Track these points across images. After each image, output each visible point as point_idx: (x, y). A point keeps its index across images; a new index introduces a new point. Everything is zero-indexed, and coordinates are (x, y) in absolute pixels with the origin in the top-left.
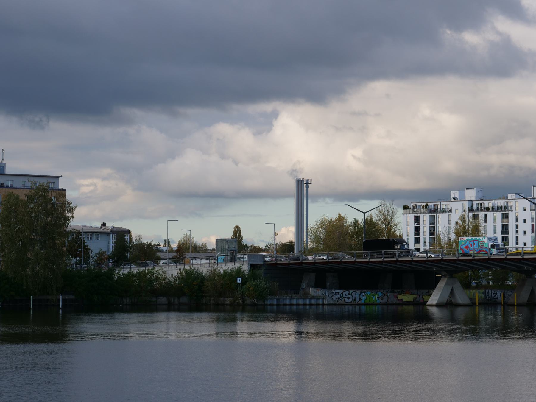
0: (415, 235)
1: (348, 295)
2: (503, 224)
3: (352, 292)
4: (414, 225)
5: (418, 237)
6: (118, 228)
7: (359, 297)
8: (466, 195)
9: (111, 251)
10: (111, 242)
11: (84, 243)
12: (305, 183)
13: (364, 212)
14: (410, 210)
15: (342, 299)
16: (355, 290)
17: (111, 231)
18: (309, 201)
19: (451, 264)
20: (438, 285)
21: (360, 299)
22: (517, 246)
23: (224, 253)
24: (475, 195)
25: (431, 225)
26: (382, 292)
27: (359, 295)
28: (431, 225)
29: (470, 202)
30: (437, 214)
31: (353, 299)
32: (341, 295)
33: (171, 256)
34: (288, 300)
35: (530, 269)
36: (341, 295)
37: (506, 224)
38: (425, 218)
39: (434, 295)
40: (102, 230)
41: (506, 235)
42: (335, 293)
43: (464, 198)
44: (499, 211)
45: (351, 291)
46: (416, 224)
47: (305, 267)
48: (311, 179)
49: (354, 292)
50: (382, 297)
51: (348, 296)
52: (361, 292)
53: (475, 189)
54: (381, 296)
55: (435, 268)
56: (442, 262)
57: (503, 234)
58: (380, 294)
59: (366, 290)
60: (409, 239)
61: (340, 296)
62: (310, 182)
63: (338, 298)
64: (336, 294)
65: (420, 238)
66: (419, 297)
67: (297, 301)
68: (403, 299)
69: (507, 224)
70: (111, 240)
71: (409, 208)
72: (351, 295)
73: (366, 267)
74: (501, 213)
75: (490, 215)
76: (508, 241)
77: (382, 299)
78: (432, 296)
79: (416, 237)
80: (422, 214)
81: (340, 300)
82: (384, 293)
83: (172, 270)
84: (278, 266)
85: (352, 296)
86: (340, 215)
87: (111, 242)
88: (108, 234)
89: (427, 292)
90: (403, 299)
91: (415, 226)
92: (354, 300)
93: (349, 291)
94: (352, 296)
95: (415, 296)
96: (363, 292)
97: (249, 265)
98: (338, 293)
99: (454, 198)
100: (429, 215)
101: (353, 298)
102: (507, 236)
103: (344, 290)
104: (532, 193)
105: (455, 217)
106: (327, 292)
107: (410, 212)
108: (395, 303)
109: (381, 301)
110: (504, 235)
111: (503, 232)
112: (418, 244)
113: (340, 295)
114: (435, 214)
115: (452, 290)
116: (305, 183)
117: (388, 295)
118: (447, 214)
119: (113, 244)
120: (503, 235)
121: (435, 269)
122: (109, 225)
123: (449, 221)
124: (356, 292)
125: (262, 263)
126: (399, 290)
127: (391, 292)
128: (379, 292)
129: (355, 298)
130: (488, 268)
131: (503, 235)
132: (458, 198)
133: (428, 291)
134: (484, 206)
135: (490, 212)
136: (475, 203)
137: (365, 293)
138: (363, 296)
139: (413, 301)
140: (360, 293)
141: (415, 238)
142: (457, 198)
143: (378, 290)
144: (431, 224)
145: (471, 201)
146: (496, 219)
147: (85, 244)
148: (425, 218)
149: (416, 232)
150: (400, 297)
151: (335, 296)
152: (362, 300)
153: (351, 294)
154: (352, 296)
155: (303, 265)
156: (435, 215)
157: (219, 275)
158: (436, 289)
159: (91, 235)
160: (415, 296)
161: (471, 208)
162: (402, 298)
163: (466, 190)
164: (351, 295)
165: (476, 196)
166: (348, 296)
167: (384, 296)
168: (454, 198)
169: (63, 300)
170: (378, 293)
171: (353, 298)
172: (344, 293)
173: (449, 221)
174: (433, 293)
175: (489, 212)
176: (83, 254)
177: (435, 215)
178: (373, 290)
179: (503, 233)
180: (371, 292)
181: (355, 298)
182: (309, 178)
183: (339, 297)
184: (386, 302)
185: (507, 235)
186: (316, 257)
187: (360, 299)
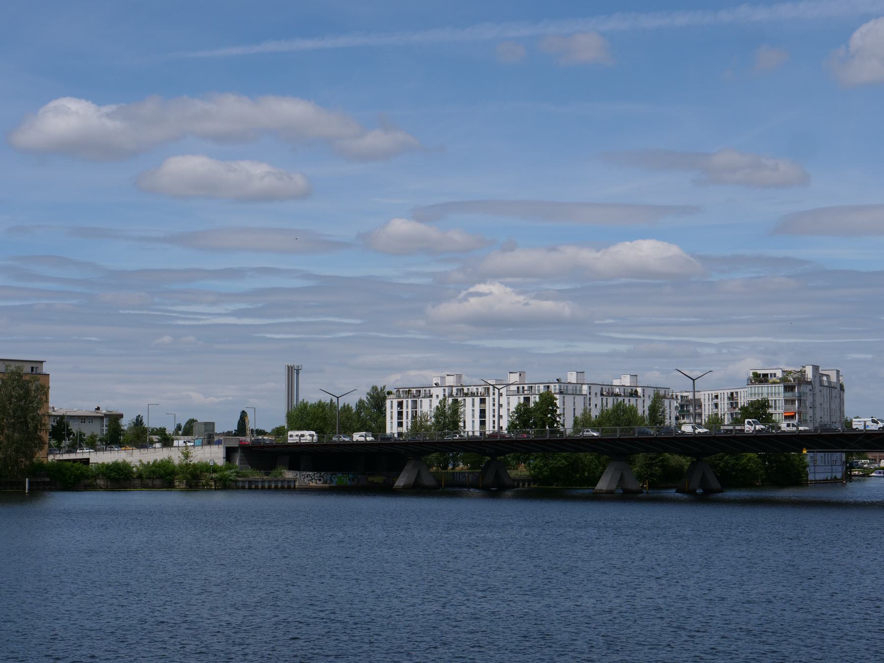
6: (112, 412)
7: (331, 479)
9: (104, 434)
10: (105, 425)
11: (68, 427)
17: (105, 415)
20: (406, 467)
29: (450, 388)
32: (313, 477)
36: (313, 477)
38: (408, 403)
40: (96, 415)
44: (634, 397)
45: (323, 473)
46: (399, 408)
51: (320, 478)
52: (332, 475)
58: (351, 476)
59: (337, 473)
62: (300, 368)
65: (485, 420)
70: (105, 424)
72: (323, 477)
74: (479, 398)
75: (469, 400)
77: (353, 480)
87: (105, 425)
88: (102, 418)
93: (321, 474)
95: (385, 478)
97: (224, 448)
98: (310, 475)
99: (435, 384)
105: (436, 403)
106: (298, 475)
109: (352, 483)
114: (417, 399)
117: (359, 477)
118: (429, 399)
119: (106, 428)
122: (103, 411)
123: (431, 406)
136: (454, 390)
138: (334, 478)
140: (330, 475)
141: (481, 421)
144: (413, 409)
145: (452, 386)
147: (69, 428)
148: (408, 403)
150: (371, 479)
155: (289, 448)
157: (105, 464)
158: (403, 471)
159: (85, 419)
160: (385, 478)
163: (447, 377)
164: (323, 477)
168: (435, 384)
169: (30, 483)
172: (316, 476)
173: (431, 406)
174: (401, 475)
179: (481, 417)
181: (327, 480)
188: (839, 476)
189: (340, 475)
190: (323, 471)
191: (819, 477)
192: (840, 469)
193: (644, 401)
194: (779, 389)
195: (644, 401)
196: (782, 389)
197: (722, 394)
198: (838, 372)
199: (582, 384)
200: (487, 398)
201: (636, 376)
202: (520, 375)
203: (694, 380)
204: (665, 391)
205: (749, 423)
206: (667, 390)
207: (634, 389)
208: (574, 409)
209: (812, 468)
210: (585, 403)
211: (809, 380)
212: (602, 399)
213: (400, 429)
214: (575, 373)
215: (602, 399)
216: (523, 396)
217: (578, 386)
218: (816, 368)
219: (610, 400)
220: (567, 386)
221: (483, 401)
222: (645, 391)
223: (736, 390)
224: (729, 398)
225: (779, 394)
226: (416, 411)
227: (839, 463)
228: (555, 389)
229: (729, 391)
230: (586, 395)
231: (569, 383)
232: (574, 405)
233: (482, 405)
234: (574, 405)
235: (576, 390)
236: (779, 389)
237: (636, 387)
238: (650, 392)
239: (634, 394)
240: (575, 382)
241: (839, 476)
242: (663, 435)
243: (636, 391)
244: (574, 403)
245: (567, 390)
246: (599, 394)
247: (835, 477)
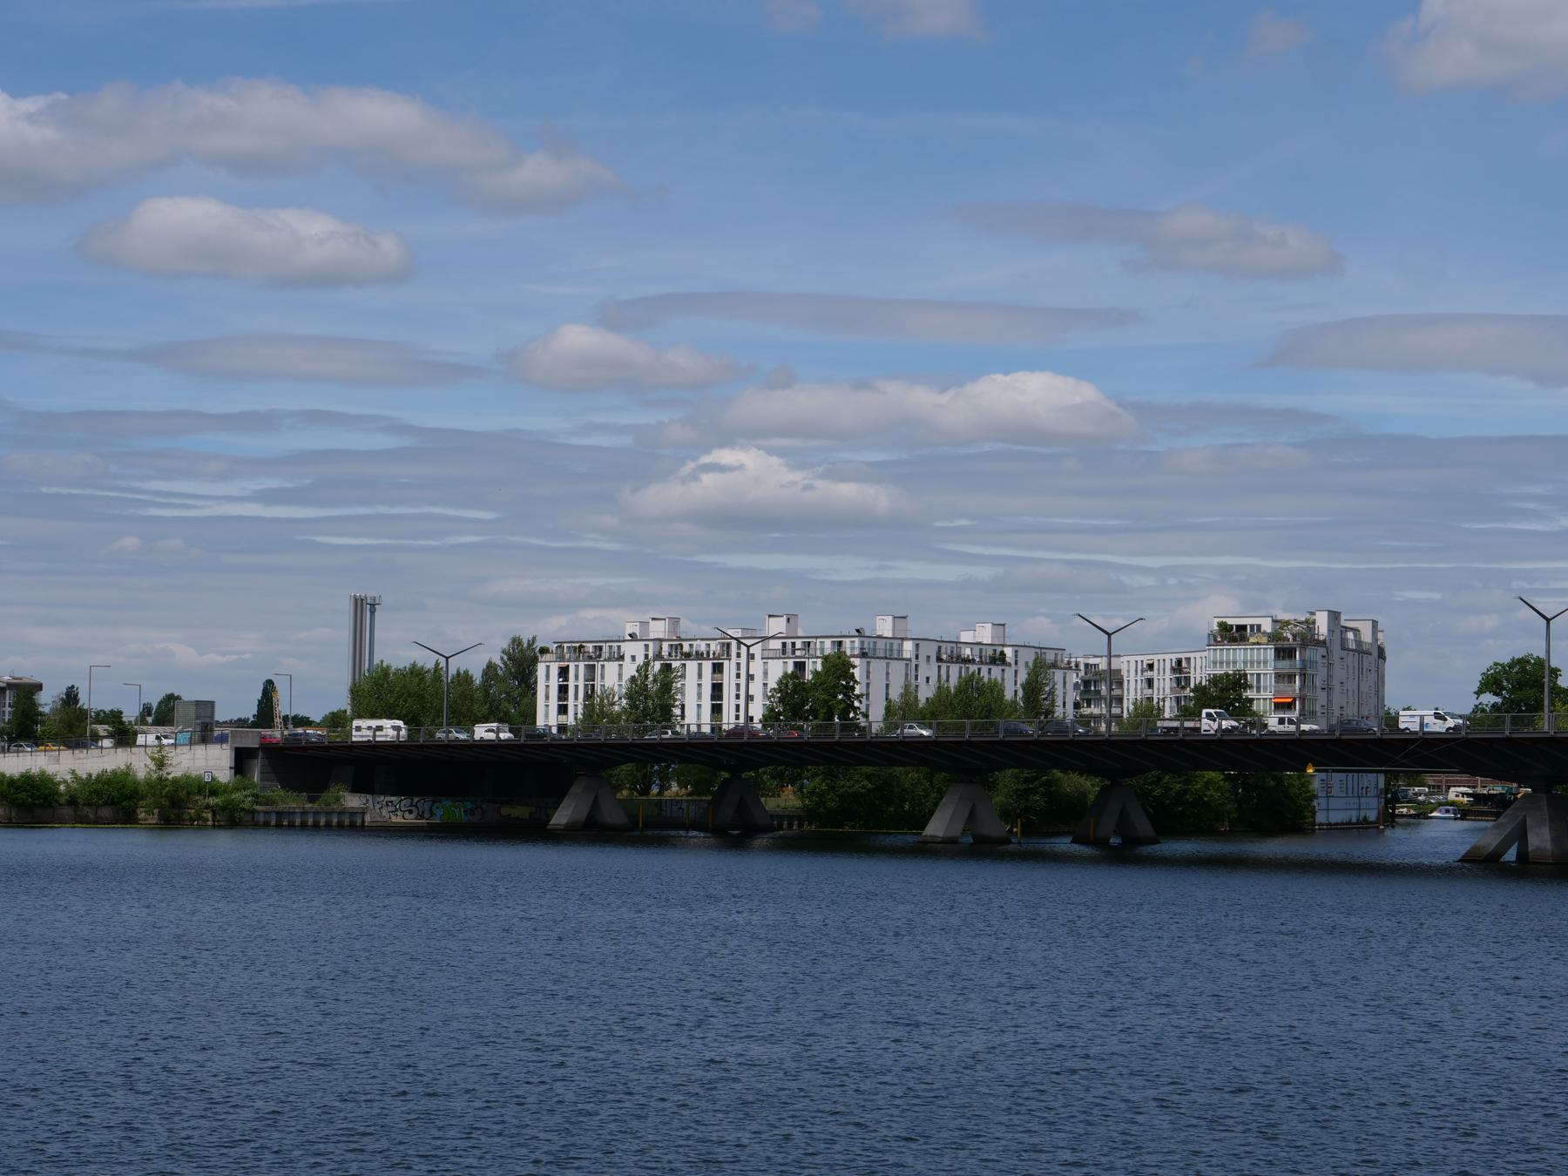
0: (712, 700)
1: (410, 806)
7: (431, 810)
8: (650, 629)
9: (6, 720)
22: (563, 719)
23: (189, 727)
24: (667, 630)
26: (472, 802)
31: (418, 814)
32: (398, 806)
33: (1462, 843)
36: (398, 806)
38: (578, 669)
43: (648, 633)
45: (416, 799)
46: (561, 680)
52: (434, 802)
56: (605, 749)
58: (469, 805)
67: (338, 818)
72: (416, 806)
77: (473, 814)
78: (560, 809)
83: (93, 757)
84: (287, 752)
93: (412, 800)
98: (391, 802)
99: (630, 635)
100: (585, 665)
102: (721, 705)
105: (630, 670)
106: (371, 801)
111: (713, 698)
114: (596, 663)
115: (596, 797)
117: (484, 806)
118: (617, 663)
119: (10, 709)
123: (620, 675)
125: (257, 746)
129: (423, 812)
136: (665, 646)
138: (437, 808)
145: (661, 640)
148: (578, 669)
150: (505, 810)
155: (332, 751)
156: (594, 665)
160: (533, 809)
164: (416, 806)
173: (620, 675)
176: (847, 829)
177: (594, 665)
181: (423, 812)
182: (377, 595)
188: (1372, 816)
189: (448, 803)
190: (416, 796)
191: (1336, 817)
192: (1373, 803)
193: (1016, 672)
194: (1265, 655)
195: (1016, 672)
196: (1271, 654)
198: (1375, 623)
199: (903, 639)
200: (726, 663)
202: (788, 620)
204: (1056, 654)
205: (1209, 716)
206: (1059, 652)
207: (999, 649)
208: (887, 686)
209: (1323, 801)
210: (907, 675)
211: (1321, 638)
212: (939, 667)
213: (563, 719)
215: (939, 667)
217: (896, 643)
218: (1334, 616)
219: (954, 669)
220: (875, 643)
221: (717, 669)
223: (1188, 655)
224: (1173, 670)
225: (1265, 662)
227: (1372, 792)
229: (1174, 657)
230: (910, 660)
231: (880, 637)
232: (887, 678)
234: (887, 678)
235: (891, 650)
236: (1265, 655)
237: (1003, 646)
238: (1028, 656)
239: (999, 659)
240: (890, 636)
241: (1372, 816)
243: (1002, 653)
244: (888, 674)
245: (875, 649)
246: (933, 658)
247: (1365, 819)
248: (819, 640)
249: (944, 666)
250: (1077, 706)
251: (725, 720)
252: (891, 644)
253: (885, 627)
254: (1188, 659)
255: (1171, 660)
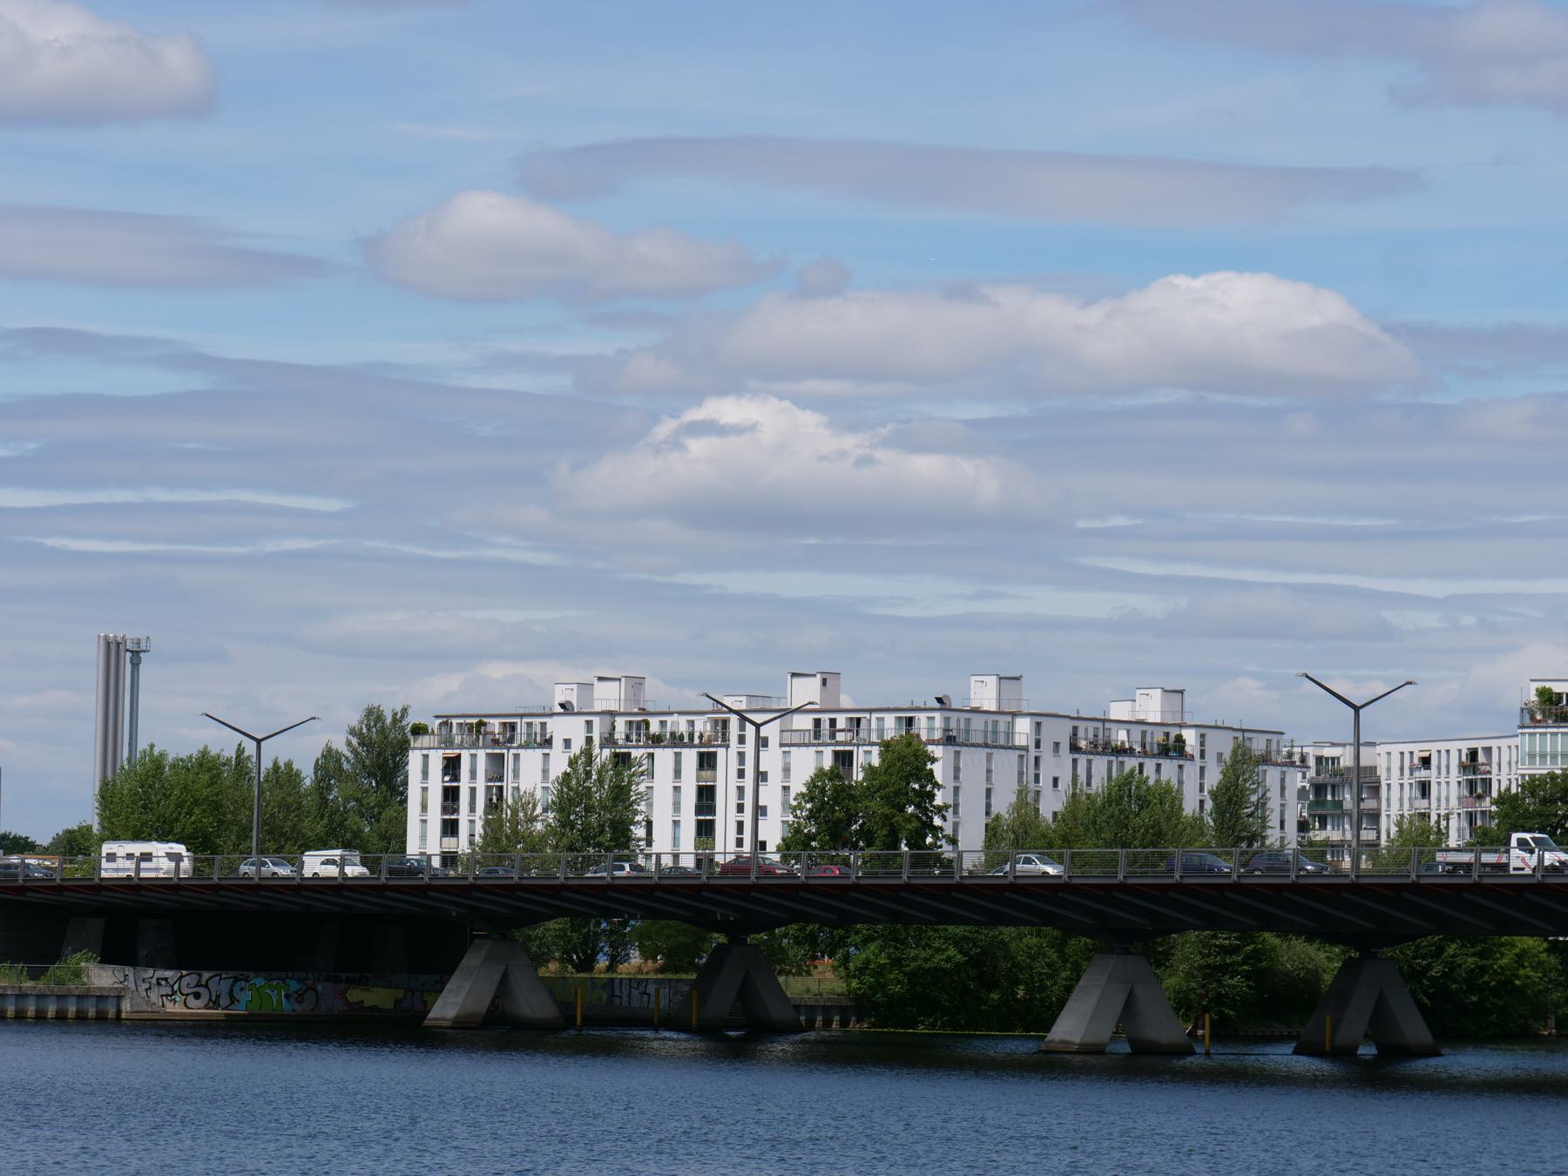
1: (197, 986)
2: (700, 784)
3: (208, 980)
4: (443, 782)
5: (452, 817)
7: (231, 994)
12: (128, 650)
13: (259, 738)
14: (432, 737)
15: (178, 999)
16: (220, 972)
18: (779, 720)
19: (454, 899)
21: (233, 1000)
24: (622, 698)
25: (492, 784)
26: (299, 980)
27: (228, 988)
28: (492, 784)
29: (608, 718)
30: (508, 750)
31: (210, 1000)
34: (110, 1000)
35: (732, 919)
37: (708, 784)
38: (475, 762)
39: (450, 991)
41: (707, 818)
42: (158, 979)
43: (591, 703)
44: (1171, 758)
45: (206, 975)
46: (447, 778)
47: (147, 900)
48: (148, 638)
49: (214, 979)
50: (300, 995)
52: (236, 980)
53: (623, 679)
54: (296, 992)
55: (455, 911)
57: (446, 815)
58: (294, 985)
59: (251, 974)
60: (679, 826)
61: (173, 989)
63: (167, 996)
64: (159, 984)
65: (457, 820)
66: (413, 995)
68: (362, 1002)
69: (712, 784)
71: (430, 731)
72: (206, 986)
73: (98, 901)
76: (714, 835)
77: (300, 998)
79: (448, 817)
80: (466, 751)
81: (171, 1000)
82: (306, 984)
85: (208, 988)
86: (206, 748)
89: (437, 982)
90: (362, 1002)
91: (446, 784)
92: (214, 1003)
93: (200, 975)
94: (206, 990)
95: (400, 993)
96: (241, 979)
98: (166, 979)
99: (562, 706)
100: (487, 754)
101: (210, 997)
103: (184, 972)
104: (789, 696)
106: (131, 977)
107: (432, 742)
108: (336, 1012)
110: (703, 818)
111: (699, 810)
112: (452, 839)
113: (172, 987)
116: (128, 650)
117: (319, 988)
120: (699, 818)
121: (454, 914)
124: (220, 979)
126: (351, 975)
127: (327, 980)
128: (292, 978)
129: (218, 997)
130: (654, 914)
131: (699, 818)
132: (575, 704)
133: (441, 978)
134: (1152, 738)
135: (664, 747)
137: (248, 982)
138: (242, 989)
139: (392, 1007)
140: (232, 980)
142: (573, 706)
143: (290, 974)
145: (612, 714)
146: (548, 771)
148: (475, 762)
149: (446, 804)
150: (354, 995)
151: (155, 989)
152: (238, 1001)
153: (204, 983)
154: (208, 988)
156: (503, 755)
160: (400, 993)
161: (610, 734)
162: (360, 999)
164: (206, 986)
165: (625, 699)
166: (196, 990)
167: (304, 992)
168: (562, 706)
170: (288, 981)
171: (210, 997)
172: (185, 981)
174: (448, 986)
175: (1168, 761)
177: (503, 755)
178: (275, 973)
179: (699, 810)
180: (266, 979)
181: (218, 997)
182: (142, 636)
183: (170, 993)
184: (313, 1010)
185: (711, 818)
186: (1017, 865)
187: (233, 1000)
189: (259, 982)
193: (1202, 769)
195: (1202, 769)
197: (1444, 754)
199: (1014, 715)
200: (721, 752)
201: (1181, 692)
202: (824, 682)
203: (1357, 709)
204: (1269, 741)
205: (1523, 844)
206: (1274, 738)
207: (1174, 732)
208: (989, 792)
210: (1021, 774)
212: (1075, 761)
213: (450, 844)
214: (992, 681)
215: (1075, 761)
216: (833, 748)
220: (968, 721)
221: (707, 762)
222: (1043, 727)
223: (1486, 743)
224: (1463, 768)
226: (500, 789)
228: (931, 729)
229: (1465, 746)
230: (1025, 749)
231: (976, 711)
232: (989, 779)
233: (706, 774)
234: (989, 779)
235: (995, 732)
237: (1181, 726)
239: (1173, 749)
240: (993, 708)
242: (1258, 878)
244: (989, 771)
245: (967, 732)
248: (874, 716)
249: (1082, 760)
250: (1303, 826)
251: (719, 847)
252: (995, 723)
253: (985, 695)
254: (1488, 750)
255: (1460, 751)
